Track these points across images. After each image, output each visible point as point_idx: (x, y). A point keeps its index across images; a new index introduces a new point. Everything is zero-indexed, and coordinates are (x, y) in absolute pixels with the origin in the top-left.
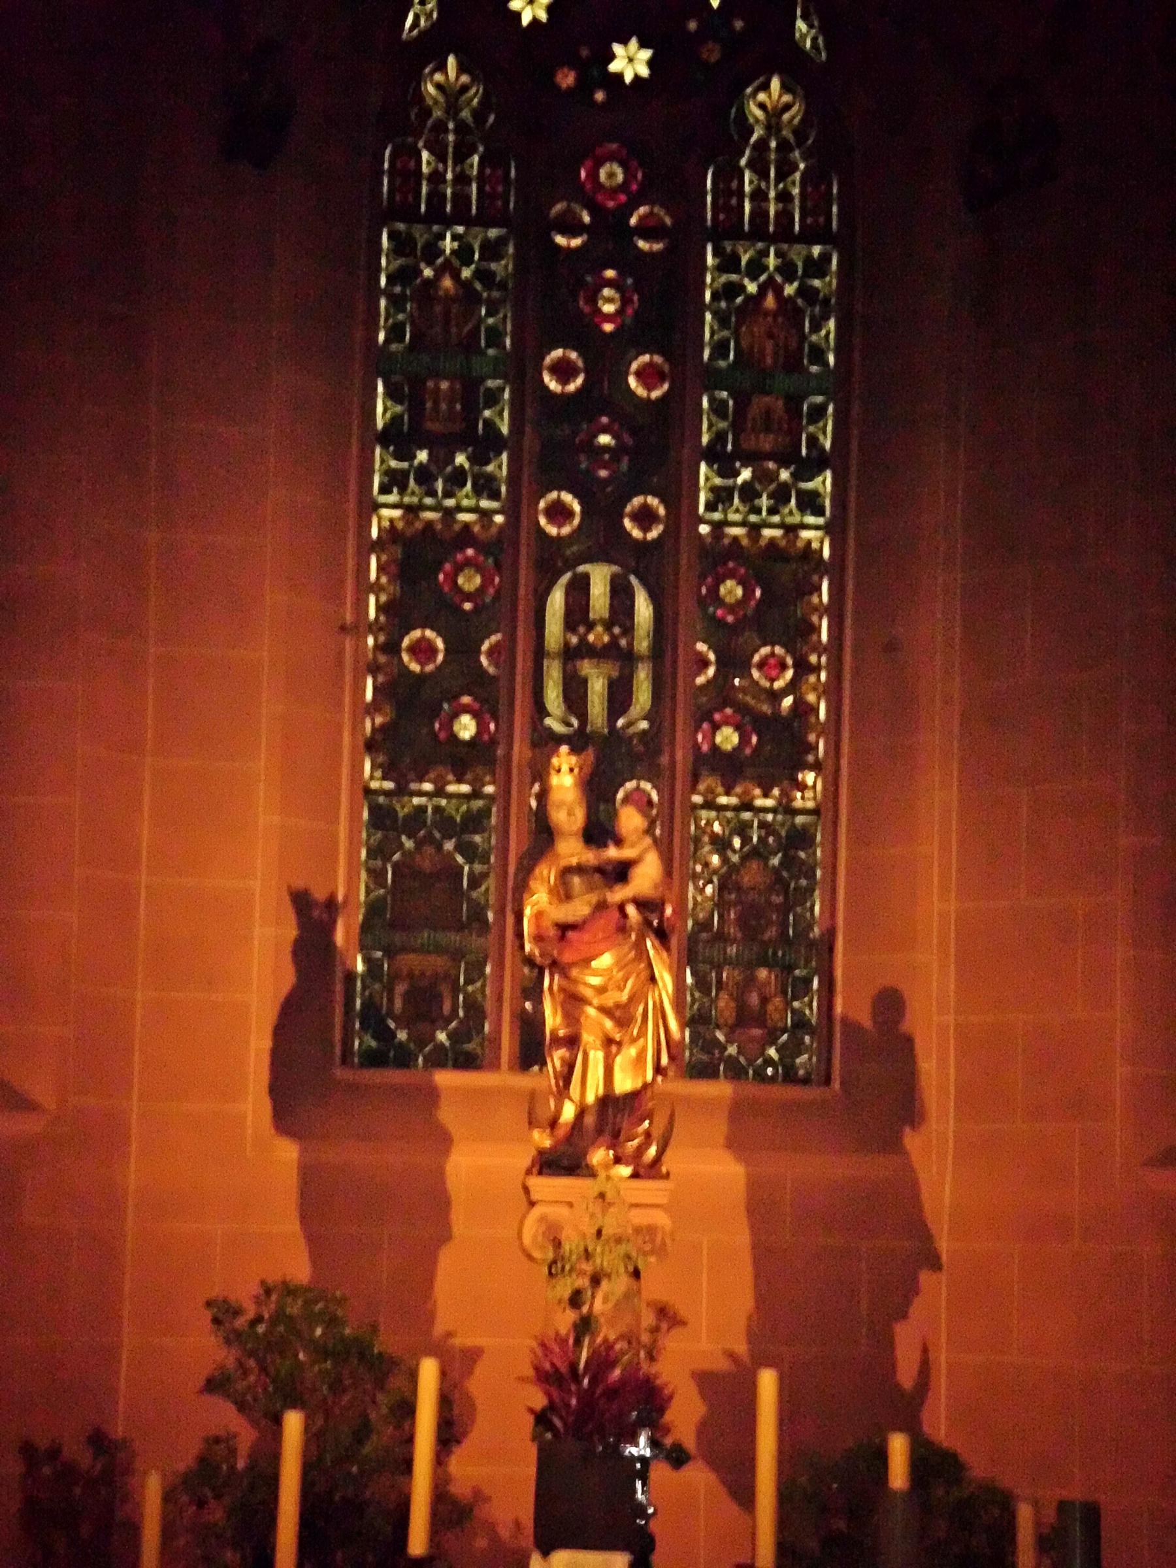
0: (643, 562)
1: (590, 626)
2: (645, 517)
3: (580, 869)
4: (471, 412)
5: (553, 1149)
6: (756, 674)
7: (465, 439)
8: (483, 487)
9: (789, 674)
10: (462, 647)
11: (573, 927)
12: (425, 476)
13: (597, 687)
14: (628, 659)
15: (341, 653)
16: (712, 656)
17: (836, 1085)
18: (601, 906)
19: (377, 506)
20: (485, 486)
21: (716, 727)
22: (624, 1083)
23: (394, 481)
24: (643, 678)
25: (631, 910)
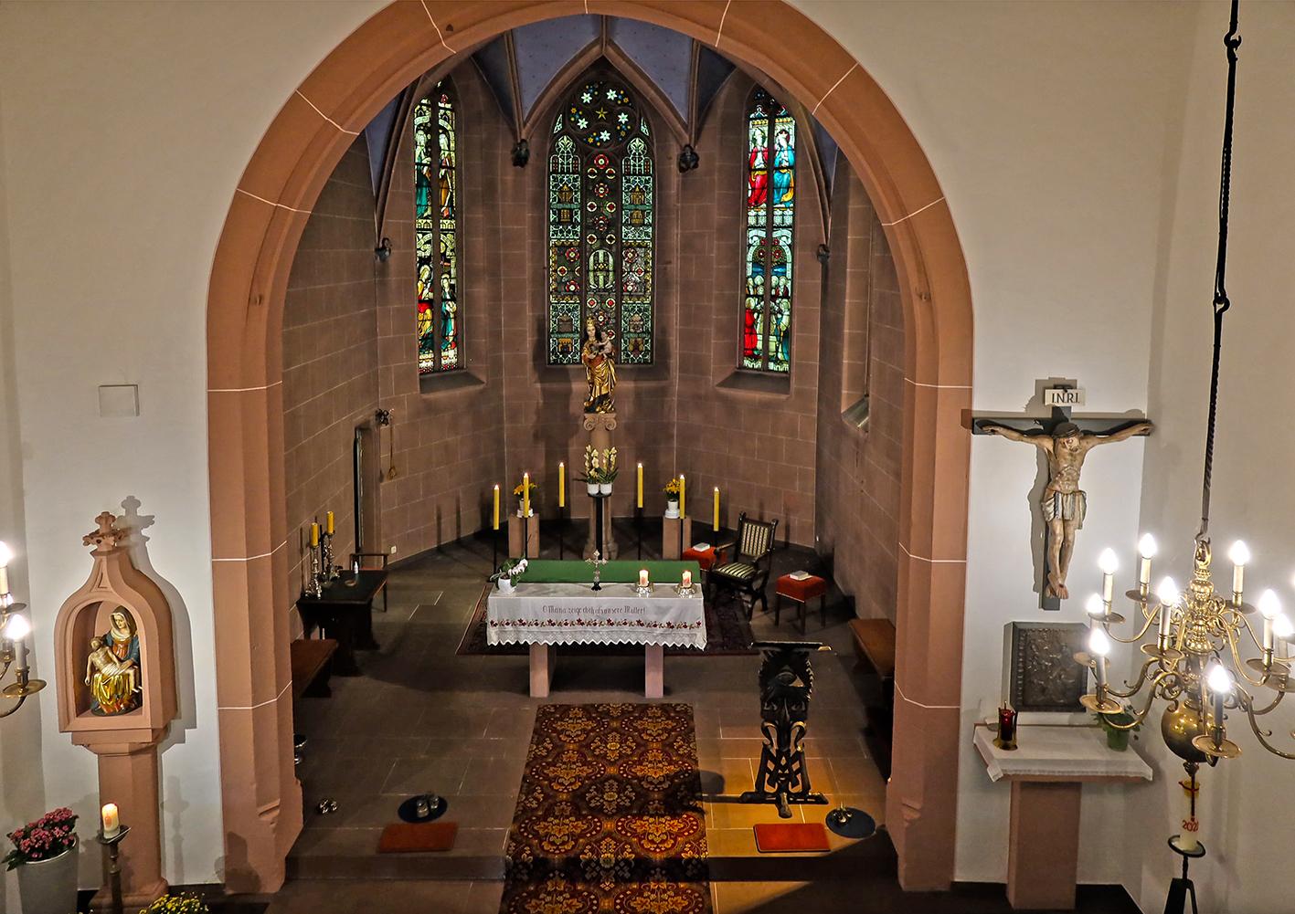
4: (571, 217)
7: (571, 223)
13: (601, 277)
14: (608, 271)
20: (575, 233)
24: (611, 274)
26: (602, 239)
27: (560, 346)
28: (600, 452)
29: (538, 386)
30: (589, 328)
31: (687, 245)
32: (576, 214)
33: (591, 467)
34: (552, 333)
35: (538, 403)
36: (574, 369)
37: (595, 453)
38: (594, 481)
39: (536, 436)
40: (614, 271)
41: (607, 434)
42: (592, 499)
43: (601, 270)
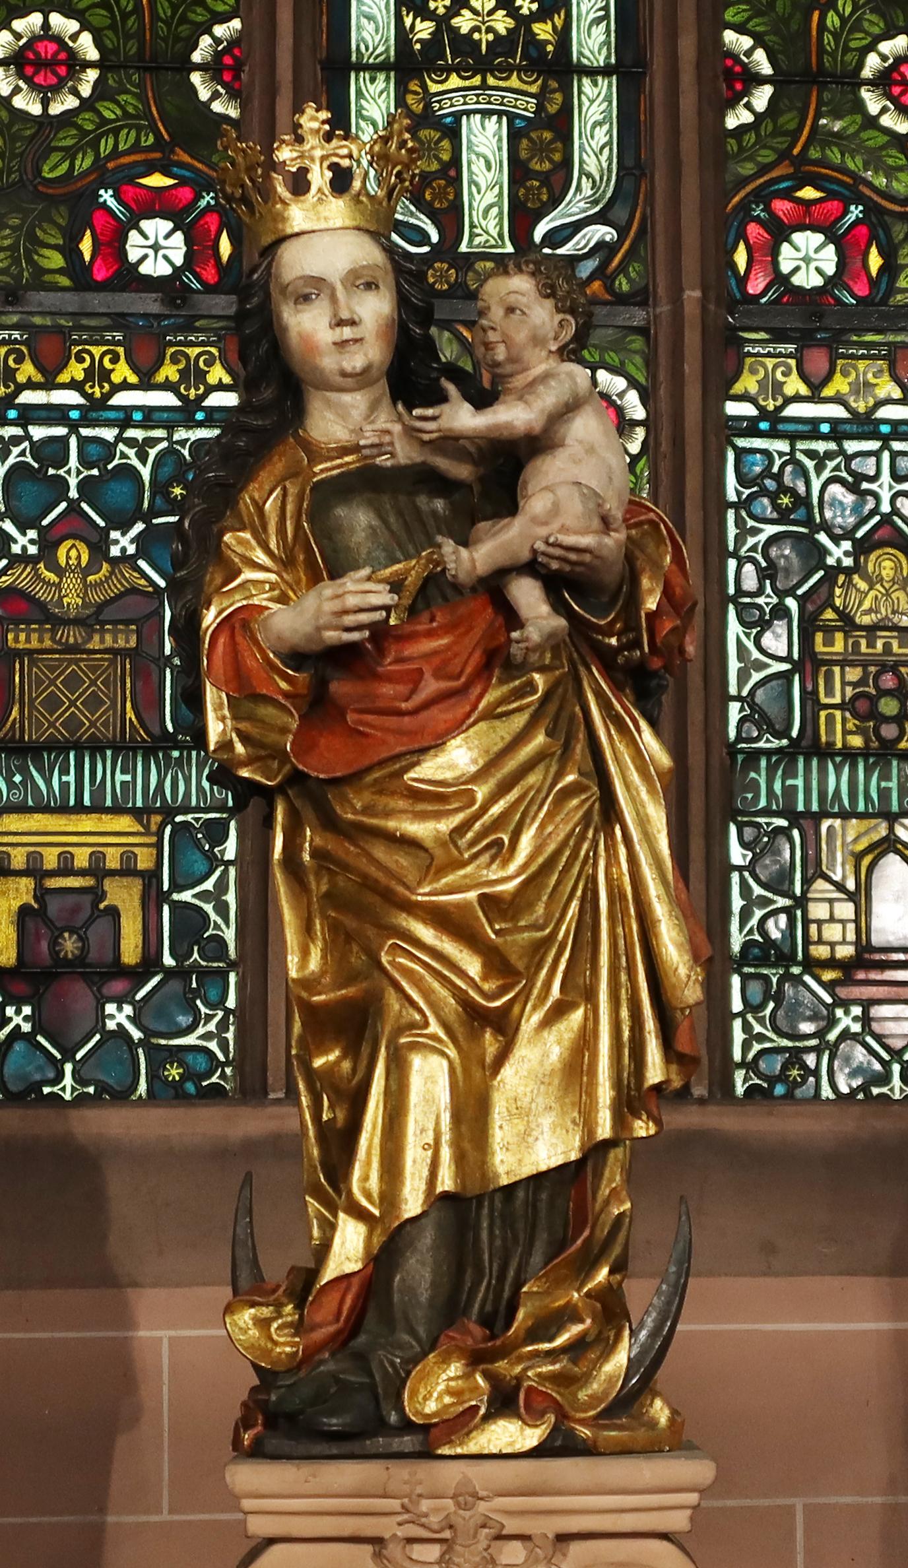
3: (367, 480)
5: (297, 1364)
6: (873, 103)
11: (342, 657)
13: (484, 144)
14: (559, 68)
16: (762, 63)
18: (435, 590)
21: (780, 232)
22: (532, 1140)
24: (595, 104)
25: (528, 596)
30: (297, 262)
40: (628, 69)
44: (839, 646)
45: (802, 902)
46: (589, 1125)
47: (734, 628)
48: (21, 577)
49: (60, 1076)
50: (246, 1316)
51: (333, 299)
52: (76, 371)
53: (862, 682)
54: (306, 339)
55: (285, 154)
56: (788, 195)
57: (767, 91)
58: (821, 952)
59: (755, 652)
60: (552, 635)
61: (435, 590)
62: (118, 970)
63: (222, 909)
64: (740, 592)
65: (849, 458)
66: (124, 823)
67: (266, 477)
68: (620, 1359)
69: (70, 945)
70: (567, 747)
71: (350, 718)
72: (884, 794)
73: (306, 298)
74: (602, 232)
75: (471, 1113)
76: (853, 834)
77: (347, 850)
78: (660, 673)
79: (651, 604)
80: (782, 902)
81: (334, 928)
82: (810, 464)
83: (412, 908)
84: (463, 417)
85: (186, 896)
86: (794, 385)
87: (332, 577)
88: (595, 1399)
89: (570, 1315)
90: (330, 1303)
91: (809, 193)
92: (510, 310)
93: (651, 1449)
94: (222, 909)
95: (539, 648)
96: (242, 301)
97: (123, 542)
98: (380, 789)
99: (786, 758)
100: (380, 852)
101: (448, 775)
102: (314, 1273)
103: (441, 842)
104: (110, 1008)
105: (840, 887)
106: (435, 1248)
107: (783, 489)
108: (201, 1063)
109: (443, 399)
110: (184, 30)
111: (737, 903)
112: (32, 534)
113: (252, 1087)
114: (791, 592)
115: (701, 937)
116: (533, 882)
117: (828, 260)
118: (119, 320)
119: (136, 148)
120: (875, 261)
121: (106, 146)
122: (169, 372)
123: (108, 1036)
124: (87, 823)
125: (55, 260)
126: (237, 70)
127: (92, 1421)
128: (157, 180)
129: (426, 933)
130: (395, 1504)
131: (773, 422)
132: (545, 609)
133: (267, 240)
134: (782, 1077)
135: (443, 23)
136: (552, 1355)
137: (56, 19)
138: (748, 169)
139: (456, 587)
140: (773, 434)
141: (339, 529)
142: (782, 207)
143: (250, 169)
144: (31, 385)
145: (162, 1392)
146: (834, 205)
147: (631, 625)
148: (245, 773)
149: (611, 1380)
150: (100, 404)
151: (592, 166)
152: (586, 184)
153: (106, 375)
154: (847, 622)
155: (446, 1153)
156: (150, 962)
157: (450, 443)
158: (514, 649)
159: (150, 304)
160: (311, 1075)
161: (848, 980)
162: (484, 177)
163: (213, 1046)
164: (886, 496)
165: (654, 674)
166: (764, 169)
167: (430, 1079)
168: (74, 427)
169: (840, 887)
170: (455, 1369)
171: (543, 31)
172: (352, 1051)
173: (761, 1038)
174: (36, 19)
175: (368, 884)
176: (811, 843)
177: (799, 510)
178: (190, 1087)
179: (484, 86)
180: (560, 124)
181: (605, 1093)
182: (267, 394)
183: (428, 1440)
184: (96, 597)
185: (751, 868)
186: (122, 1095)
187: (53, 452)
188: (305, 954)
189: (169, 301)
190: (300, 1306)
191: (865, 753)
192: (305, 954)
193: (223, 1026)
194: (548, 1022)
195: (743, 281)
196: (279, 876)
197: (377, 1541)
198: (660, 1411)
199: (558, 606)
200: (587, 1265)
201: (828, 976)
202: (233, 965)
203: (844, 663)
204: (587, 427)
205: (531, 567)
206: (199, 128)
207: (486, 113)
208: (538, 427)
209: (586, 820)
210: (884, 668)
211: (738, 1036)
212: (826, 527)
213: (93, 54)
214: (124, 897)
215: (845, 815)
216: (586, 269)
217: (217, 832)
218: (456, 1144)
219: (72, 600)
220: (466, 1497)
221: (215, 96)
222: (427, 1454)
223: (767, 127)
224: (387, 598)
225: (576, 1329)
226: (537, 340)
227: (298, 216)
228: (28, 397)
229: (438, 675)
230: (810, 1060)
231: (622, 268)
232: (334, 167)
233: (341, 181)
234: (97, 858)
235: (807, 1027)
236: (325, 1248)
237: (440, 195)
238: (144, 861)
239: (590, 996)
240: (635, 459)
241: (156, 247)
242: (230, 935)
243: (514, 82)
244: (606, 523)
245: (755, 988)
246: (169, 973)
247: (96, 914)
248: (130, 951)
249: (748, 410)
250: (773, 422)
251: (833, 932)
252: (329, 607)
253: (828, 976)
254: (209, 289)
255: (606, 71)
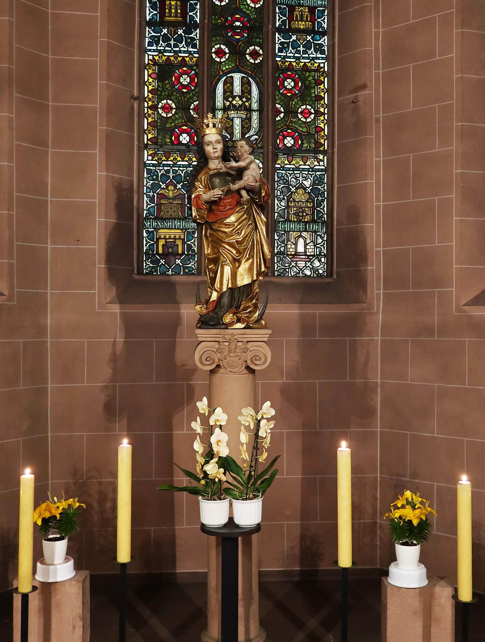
0: (255, 72)
1: (234, 98)
2: (255, 55)
3: (219, 174)
4: (184, 14)
5: (206, 314)
7: (182, 24)
8: (189, 43)
9: (312, 116)
10: (183, 107)
12: (166, 38)
13: (237, 122)
14: (249, 110)
15: (132, 108)
17: (335, 276)
18: (229, 192)
19: (146, 51)
20: (191, 42)
21: (285, 137)
22: (244, 280)
23: (155, 41)
24: (255, 116)
25: (244, 193)
26: (237, 53)
27: (162, 242)
28: (233, 415)
29: (116, 309)
30: (207, 139)
31: (396, 51)
32: (193, 9)
33: (209, 455)
34: (147, 218)
35: (114, 342)
36: (186, 284)
37: (219, 416)
38: (216, 491)
39: (110, 409)
40: (260, 110)
41: (247, 377)
42: (213, 538)
43: (236, 108)
44: (293, 204)
45: (286, 245)
46: (252, 277)
47: (276, 201)
48: (163, 192)
49: (169, 271)
50: (198, 307)
51: (213, 145)
52: (172, 158)
53: (297, 210)
54: (209, 151)
55: (205, 121)
56: (286, 131)
57: (283, 114)
58: (289, 253)
59: (279, 205)
60: (248, 199)
61: (229, 192)
62: (178, 254)
63: (195, 245)
64: (277, 195)
65: (295, 174)
66: (179, 231)
67: (202, 173)
68: (257, 314)
69: (170, 250)
70: (250, 217)
71: (215, 212)
72: (300, 228)
73: (209, 145)
74: (257, 137)
75: (234, 275)
76: (294, 234)
77: (215, 233)
78: (265, 207)
79: (263, 195)
80: (283, 245)
81: (212, 246)
82: (289, 175)
83: (225, 243)
84: (234, 164)
85: (189, 243)
86: (286, 162)
87: (213, 190)
88: (253, 320)
89: (249, 307)
90: (211, 304)
91: (289, 131)
92: (241, 147)
93: (261, 328)
94: (195, 245)
95: (245, 201)
96: (198, 147)
97: (179, 186)
98: (220, 223)
99: (284, 222)
100: (220, 234)
101: (231, 222)
102: (209, 300)
103: (229, 232)
104: (177, 260)
105: (292, 243)
106: (228, 296)
107: (284, 179)
108: (191, 269)
109: (230, 161)
110: (189, 103)
111: (276, 245)
112: (165, 185)
113: (199, 273)
114: (285, 196)
115: (271, 248)
116: (244, 239)
117: (292, 142)
118: (179, 150)
119: (181, 122)
120: (300, 142)
121: (176, 122)
122: (186, 159)
123: (176, 265)
124: (173, 231)
125: (168, 140)
126: (197, 110)
127: (173, 325)
128: (185, 128)
129: (227, 247)
130: (221, 336)
131: (283, 168)
132: (246, 195)
133: (202, 135)
134: (283, 273)
135: (231, 102)
136: (246, 313)
137: (168, 101)
138: (279, 127)
139: (232, 191)
140: (283, 170)
141: (214, 182)
142: (285, 133)
143: (200, 124)
144: (164, 161)
145: (185, 320)
146: (294, 133)
147: (260, 198)
148: (198, 221)
149: (255, 317)
150: (176, 164)
151: (254, 126)
152: (254, 129)
153: (176, 159)
154: (294, 201)
155: (230, 281)
156: (183, 253)
157: (232, 168)
158: (242, 201)
159: (183, 148)
160: (208, 269)
161: (293, 258)
162: (237, 128)
163: (193, 266)
164: (301, 180)
165: (264, 206)
166: (282, 127)
167: (227, 270)
168: (171, 167)
169: (292, 243)
170: (231, 315)
171: (247, 104)
172: (215, 265)
173: (280, 267)
174: (165, 101)
175: (218, 239)
176: (288, 236)
177: (287, 182)
178: (189, 273)
179: (237, 113)
180: (250, 119)
181: (255, 272)
182: (202, 160)
183: (227, 326)
184: (175, 195)
185: (278, 240)
186: (179, 274)
187: (168, 171)
188: (208, 250)
189: (186, 147)
190: (207, 305)
191: (297, 221)
192: (208, 250)
193: (195, 263)
194: (246, 261)
195: (278, 145)
196: (204, 237)
197: (218, 342)
198: (263, 322)
199: (249, 195)
200: (252, 299)
201: (290, 257)
202: (196, 254)
203: (294, 207)
204: (253, 166)
205: (244, 188)
206: (191, 119)
207: (238, 117)
208: (245, 166)
209: (253, 229)
210: (300, 208)
211: (276, 266)
212: (291, 185)
213: (174, 107)
214: (179, 243)
215: (293, 231)
216: (254, 142)
217: (194, 233)
218: (231, 280)
219: (171, 195)
220: (233, 335)
221: (194, 114)
222: (227, 328)
223: (283, 120)
224: (222, 193)
225: (250, 309)
226: (246, 152)
227: (207, 131)
228: (164, 162)
229: (229, 206)
230: (287, 270)
231: (259, 143)
232: (213, 123)
233: (214, 126)
234: (175, 236)
235: (287, 265)
236: (211, 296)
237: (230, 130)
238: (182, 237)
239: (253, 257)
240: (261, 174)
241: (185, 139)
242: (196, 249)
243: (242, 112)
244: (256, 181)
245: (279, 259)
246: (186, 255)
247: (175, 245)
248: (180, 251)
249: (279, 166)
250: (283, 168)
251: (291, 250)
252: (212, 194)
253: (290, 257)
254: (193, 145)
255: (257, 111)
